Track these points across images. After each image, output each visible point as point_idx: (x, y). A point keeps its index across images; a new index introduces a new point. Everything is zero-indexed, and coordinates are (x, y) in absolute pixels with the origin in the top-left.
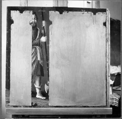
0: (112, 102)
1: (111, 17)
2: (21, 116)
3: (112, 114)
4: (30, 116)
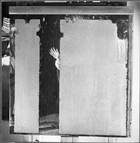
3: (10, 7)
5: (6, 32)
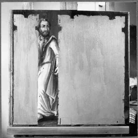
5: (132, 109)
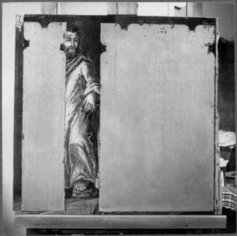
0: (225, 202)
1: (221, 37)
2: (45, 232)
4: (62, 231)
5: (231, 186)
